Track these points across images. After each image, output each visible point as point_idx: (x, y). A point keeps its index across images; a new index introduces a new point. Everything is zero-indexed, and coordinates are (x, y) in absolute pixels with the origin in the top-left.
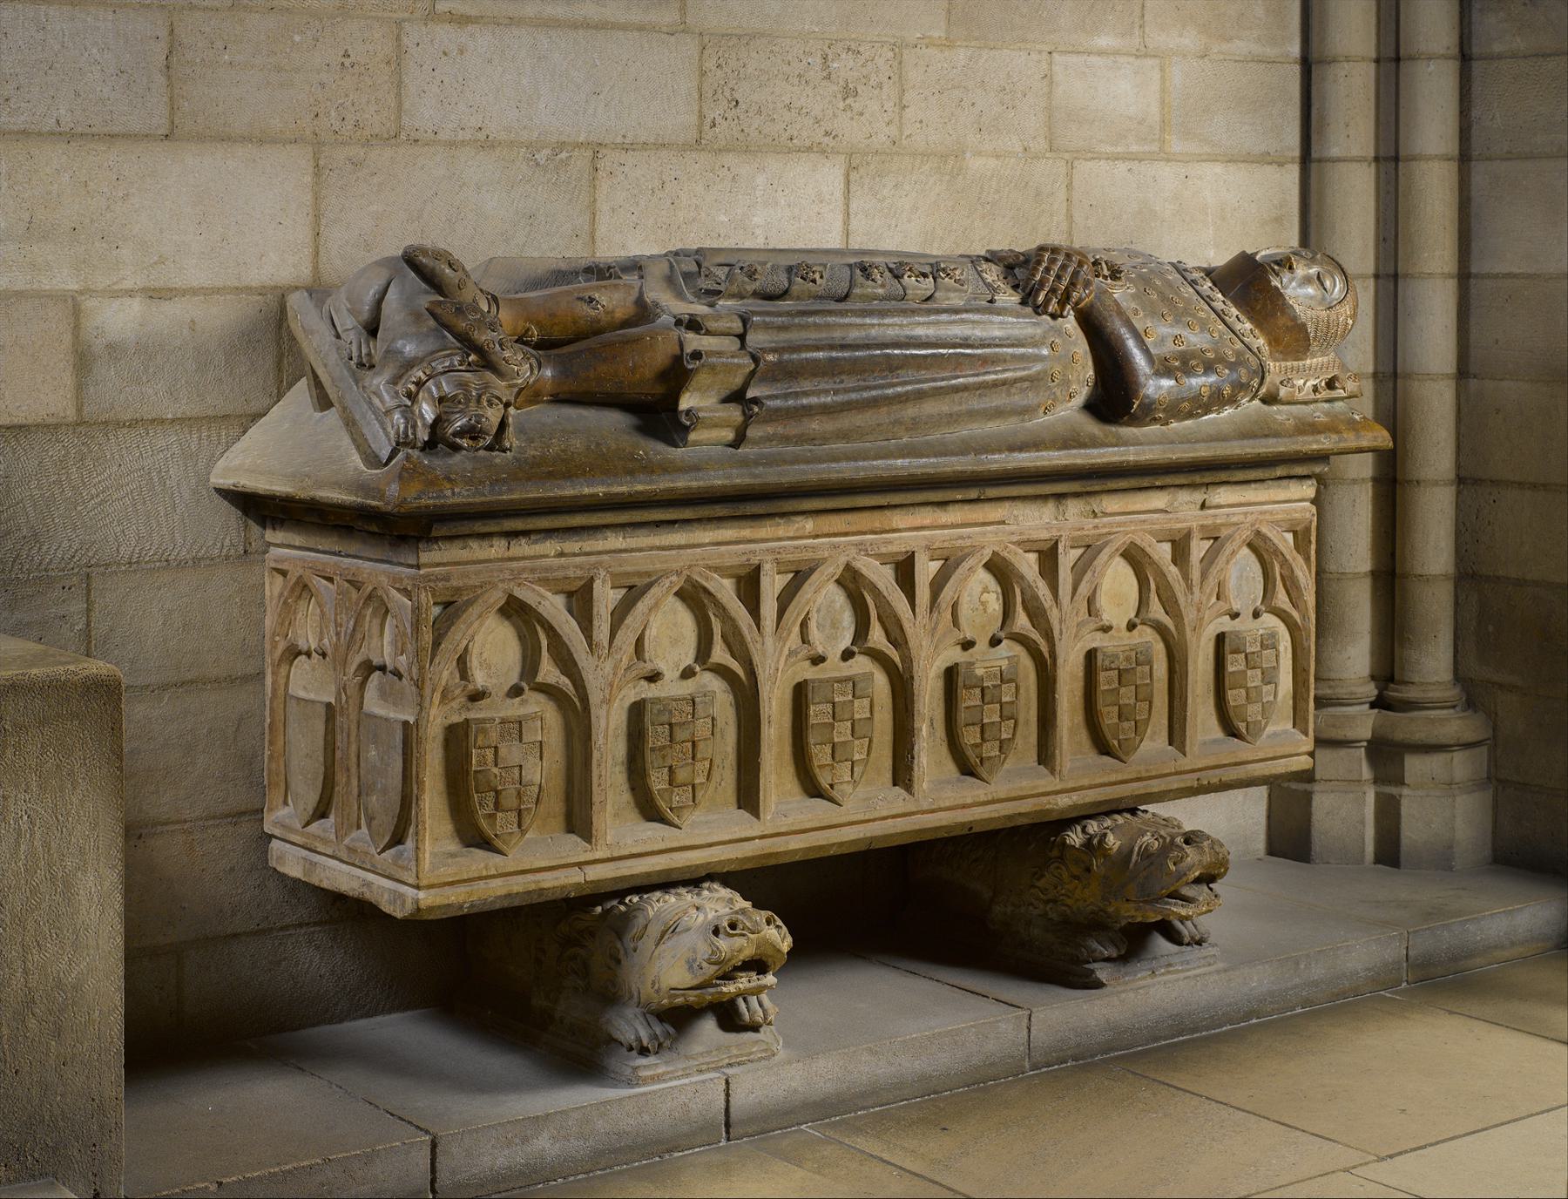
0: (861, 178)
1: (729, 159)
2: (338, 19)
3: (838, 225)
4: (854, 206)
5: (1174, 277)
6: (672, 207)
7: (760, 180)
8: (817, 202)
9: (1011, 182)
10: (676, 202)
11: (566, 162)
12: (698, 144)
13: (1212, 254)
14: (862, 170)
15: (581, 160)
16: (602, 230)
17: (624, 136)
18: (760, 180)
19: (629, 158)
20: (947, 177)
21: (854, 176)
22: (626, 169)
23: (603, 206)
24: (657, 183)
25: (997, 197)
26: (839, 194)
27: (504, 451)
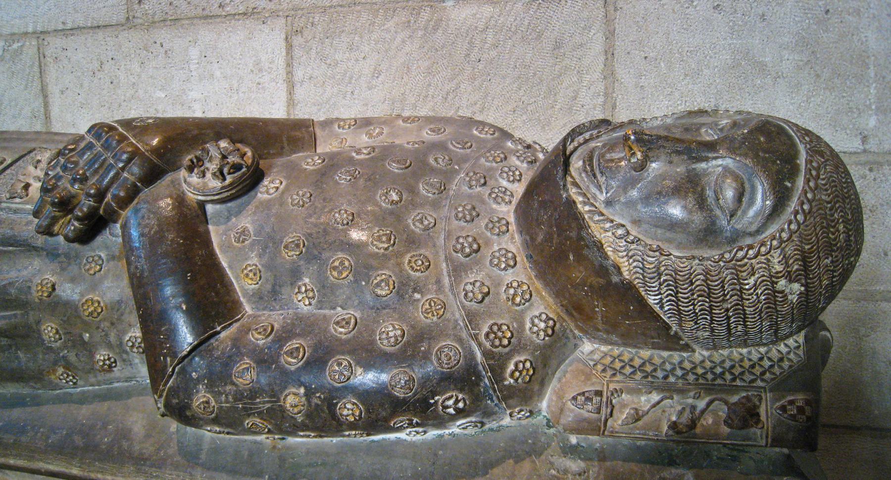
0: (307, 42)
1: (163, 35)
2: (680, 230)
3: (283, 95)
4: (299, 74)
5: (679, 121)
6: (111, 86)
7: (194, 53)
8: (256, 71)
9: (515, 33)
10: (115, 81)
11: (19, 52)
12: (129, 23)
13: (872, 122)
14: (306, 33)
15: (30, 48)
16: (55, 111)
17: (63, 23)
18: (194, 53)
19: (71, 42)
20: (420, 33)
21: (297, 40)
22: (69, 54)
23: (54, 90)
24: (97, 65)
25: (493, 53)
26: (281, 62)
27: (549, 445)
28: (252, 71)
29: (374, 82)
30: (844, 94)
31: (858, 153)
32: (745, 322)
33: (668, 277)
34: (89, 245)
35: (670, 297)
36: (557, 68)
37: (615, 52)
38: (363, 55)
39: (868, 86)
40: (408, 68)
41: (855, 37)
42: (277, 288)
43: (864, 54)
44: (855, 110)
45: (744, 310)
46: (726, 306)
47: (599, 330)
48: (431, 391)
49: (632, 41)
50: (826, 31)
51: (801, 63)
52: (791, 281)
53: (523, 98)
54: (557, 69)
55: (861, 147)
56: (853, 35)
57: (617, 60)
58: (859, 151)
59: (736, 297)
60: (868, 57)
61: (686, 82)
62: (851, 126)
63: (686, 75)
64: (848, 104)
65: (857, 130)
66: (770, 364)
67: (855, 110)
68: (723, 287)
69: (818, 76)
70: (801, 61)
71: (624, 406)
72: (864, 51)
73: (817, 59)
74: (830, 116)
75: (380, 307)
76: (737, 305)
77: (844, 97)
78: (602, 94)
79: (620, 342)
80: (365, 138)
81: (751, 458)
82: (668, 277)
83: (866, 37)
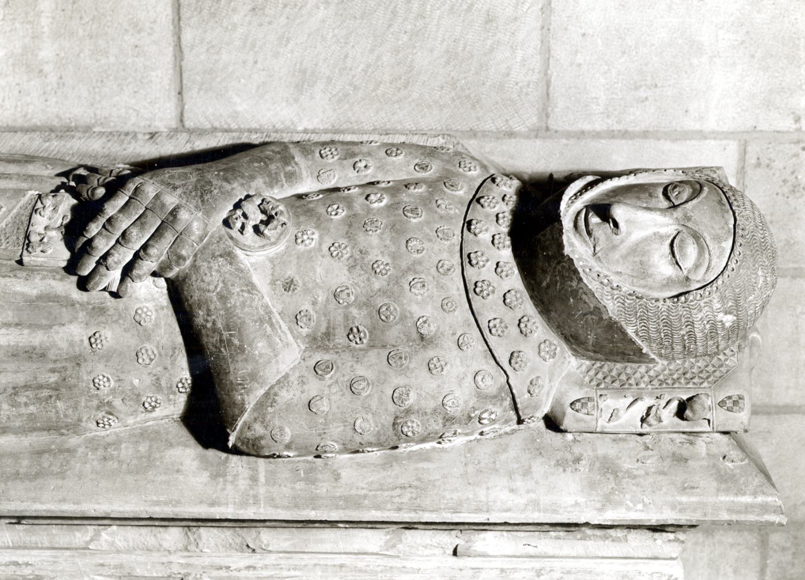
4: (187, 36)
28: (126, 30)
29: (282, 50)
30: (777, 75)
31: (791, 132)
32: (696, 343)
33: (642, 314)
34: (65, 274)
35: (643, 328)
36: (489, 42)
37: (551, 27)
38: (267, 19)
39: (799, 67)
40: (322, 36)
41: (786, 19)
42: (331, 330)
43: (794, 36)
44: (787, 90)
45: (695, 335)
46: (682, 332)
47: (589, 351)
48: (473, 407)
49: (568, 17)
50: (759, 12)
51: (736, 43)
52: (726, 314)
53: (452, 74)
54: (489, 44)
55: (794, 126)
56: (784, 17)
57: (553, 35)
58: (791, 130)
59: (689, 327)
60: (799, 39)
61: (623, 60)
62: (783, 106)
63: (624, 53)
64: (780, 84)
65: (789, 109)
66: (713, 369)
67: (787, 90)
68: (681, 320)
69: (753, 56)
70: (736, 40)
71: (608, 407)
72: (794, 33)
73: (752, 39)
74: (763, 95)
75: (448, 350)
76: (690, 331)
77: (776, 77)
78: (536, 71)
79: (603, 358)
80: (352, 174)
81: (703, 441)
82: (642, 314)
83: (796, 19)
